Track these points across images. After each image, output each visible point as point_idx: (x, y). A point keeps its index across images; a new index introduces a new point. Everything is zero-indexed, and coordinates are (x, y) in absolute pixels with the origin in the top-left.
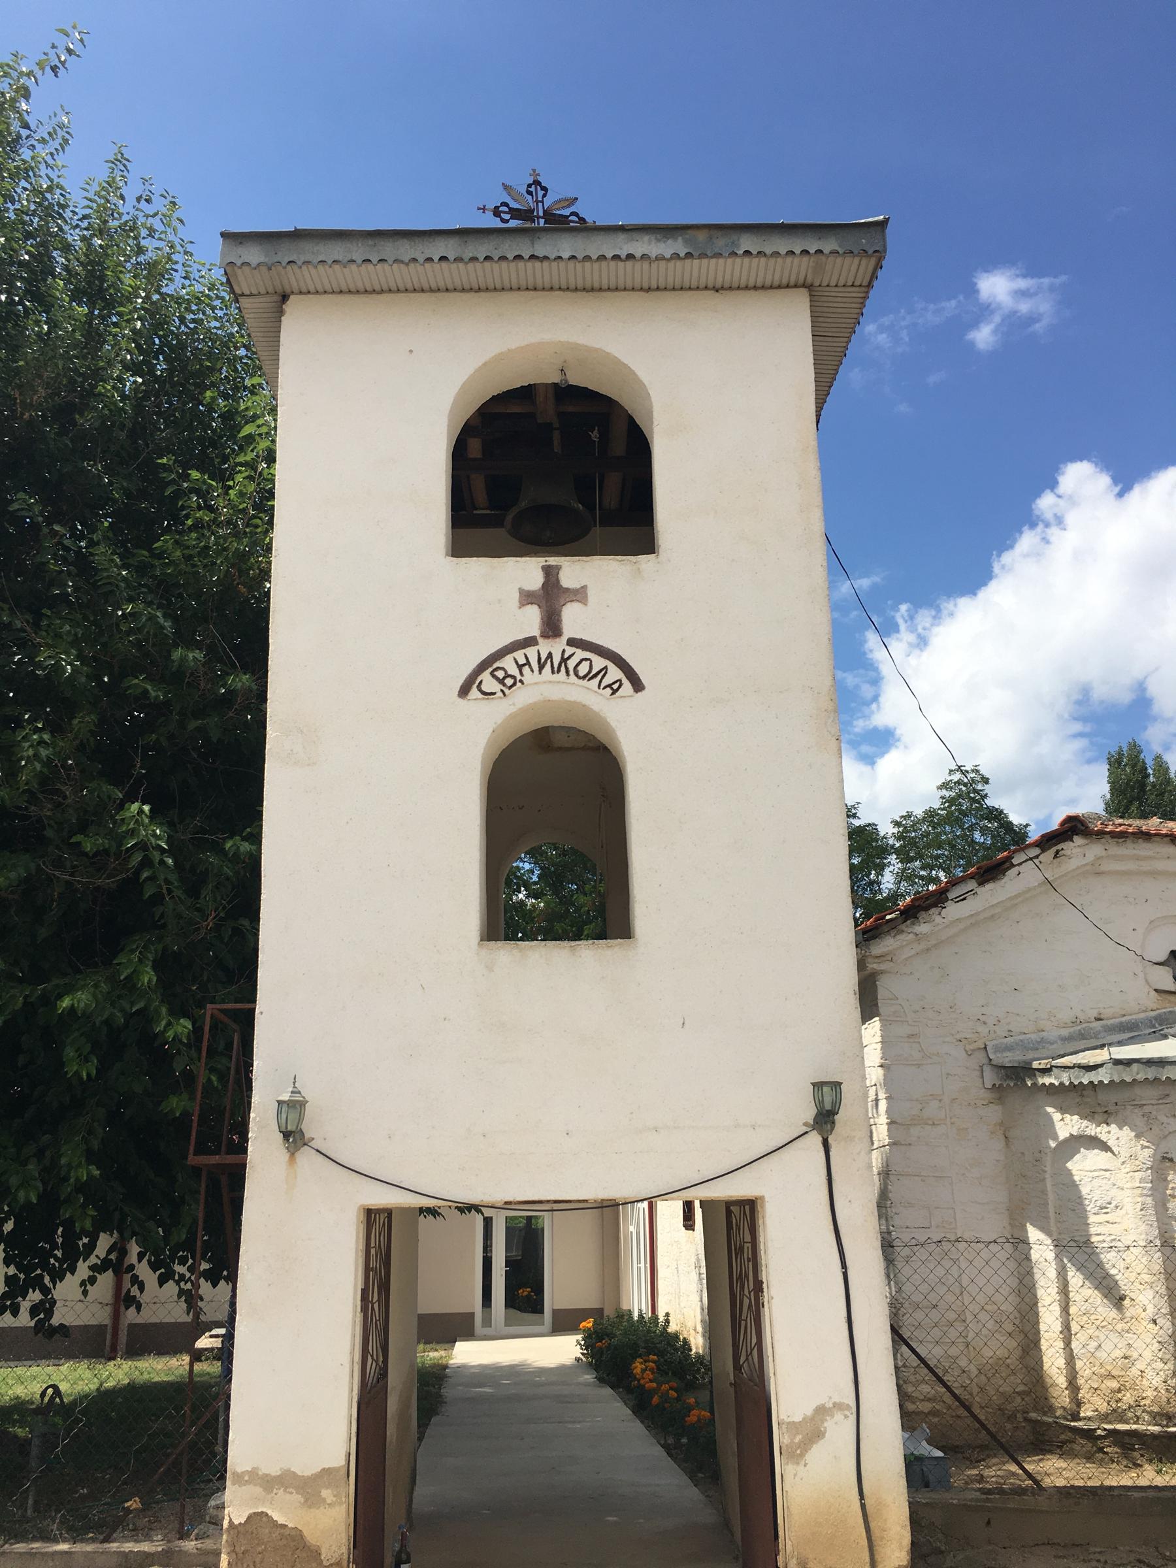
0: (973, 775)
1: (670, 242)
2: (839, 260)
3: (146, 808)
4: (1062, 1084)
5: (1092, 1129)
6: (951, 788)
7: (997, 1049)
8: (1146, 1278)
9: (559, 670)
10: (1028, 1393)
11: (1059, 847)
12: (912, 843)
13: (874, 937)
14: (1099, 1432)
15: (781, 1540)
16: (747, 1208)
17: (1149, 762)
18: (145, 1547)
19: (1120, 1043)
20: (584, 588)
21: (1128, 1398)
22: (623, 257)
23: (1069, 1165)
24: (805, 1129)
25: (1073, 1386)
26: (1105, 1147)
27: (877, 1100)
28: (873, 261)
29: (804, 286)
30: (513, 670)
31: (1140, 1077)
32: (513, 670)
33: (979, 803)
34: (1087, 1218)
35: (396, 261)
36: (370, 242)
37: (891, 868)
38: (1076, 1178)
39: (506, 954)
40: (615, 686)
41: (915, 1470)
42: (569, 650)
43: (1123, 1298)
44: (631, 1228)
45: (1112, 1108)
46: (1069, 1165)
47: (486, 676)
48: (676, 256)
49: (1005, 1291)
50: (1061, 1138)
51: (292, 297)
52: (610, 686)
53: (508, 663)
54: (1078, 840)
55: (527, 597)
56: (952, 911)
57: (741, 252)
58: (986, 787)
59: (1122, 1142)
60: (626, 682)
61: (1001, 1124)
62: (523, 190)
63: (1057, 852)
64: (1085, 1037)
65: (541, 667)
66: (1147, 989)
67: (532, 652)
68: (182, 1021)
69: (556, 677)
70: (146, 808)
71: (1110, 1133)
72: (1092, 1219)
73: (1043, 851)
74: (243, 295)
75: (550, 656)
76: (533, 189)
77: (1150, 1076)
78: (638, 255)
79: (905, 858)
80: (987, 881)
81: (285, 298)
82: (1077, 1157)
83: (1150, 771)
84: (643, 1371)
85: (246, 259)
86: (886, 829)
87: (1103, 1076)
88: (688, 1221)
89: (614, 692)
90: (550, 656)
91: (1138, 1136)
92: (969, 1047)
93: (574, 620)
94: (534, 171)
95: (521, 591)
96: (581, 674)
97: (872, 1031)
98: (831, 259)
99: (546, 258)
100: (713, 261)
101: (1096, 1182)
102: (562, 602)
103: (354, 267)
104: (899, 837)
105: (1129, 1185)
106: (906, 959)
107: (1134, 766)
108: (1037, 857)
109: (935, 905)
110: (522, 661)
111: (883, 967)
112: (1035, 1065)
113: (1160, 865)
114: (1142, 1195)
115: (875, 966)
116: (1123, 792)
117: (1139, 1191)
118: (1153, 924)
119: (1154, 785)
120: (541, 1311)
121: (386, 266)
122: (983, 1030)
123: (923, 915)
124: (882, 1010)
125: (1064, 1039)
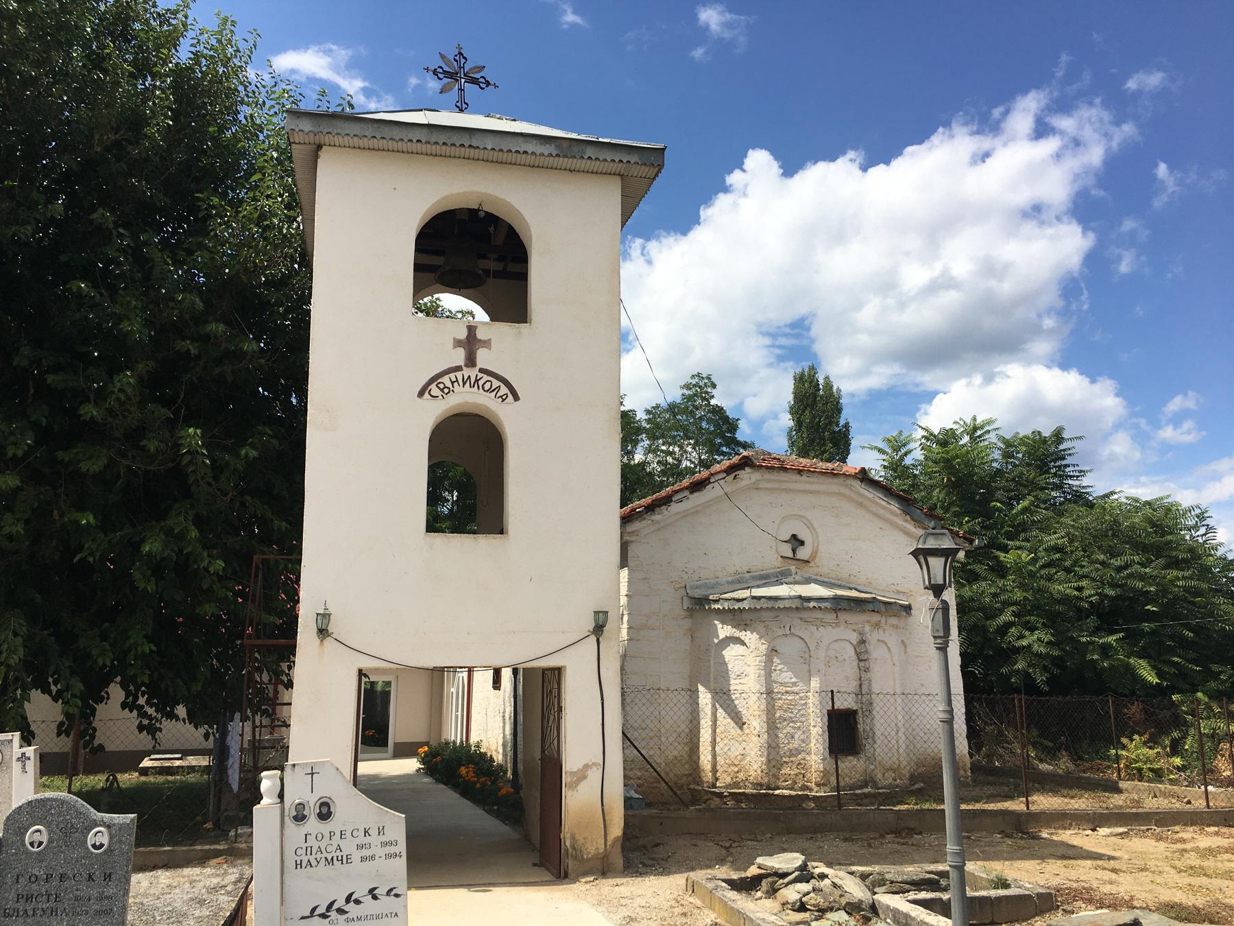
0: (706, 381)
1: (547, 146)
2: (639, 167)
3: (198, 431)
4: (724, 608)
5: (737, 634)
6: (690, 389)
7: (692, 588)
8: (757, 713)
9: (474, 386)
10: (690, 775)
11: (737, 473)
12: (658, 426)
13: (629, 521)
14: (725, 794)
15: (563, 826)
16: (556, 672)
17: (821, 381)
18: (218, 847)
19: (758, 586)
20: (490, 340)
21: (741, 775)
22: (521, 152)
23: (724, 653)
24: (588, 634)
25: (714, 770)
26: (743, 643)
27: (623, 615)
28: (657, 169)
29: (619, 175)
30: (449, 384)
31: (764, 606)
32: (449, 384)
33: (707, 400)
34: (729, 681)
35: (391, 139)
36: (376, 126)
37: (642, 444)
38: (727, 660)
39: (438, 539)
40: (504, 397)
41: (628, 802)
42: (480, 375)
43: (744, 724)
44: (452, 690)
45: (749, 622)
46: (724, 653)
47: (433, 386)
48: (551, 155)
49: (683, 718)
50: (720, 638)
51: (324, 147)
52: (501, 397)
53: (446, 380)
54: (748, 470)
55: (458, 343)
56: (675, 508)
57: (586, 157)
58: (714, 390)
59: (752, 641)
60: (509, 394)
61: (690, 629)
62: (452, 59)
63: (736, 476)
64: (740, 582)
65: (464, 384)
66: (776, 556)
67: (459, 375)
68: (218, 561)
69: (472, 389)
70: (198, 431)
71: (747, 636)
72: (732, 682)
73: (728, 475)
74: (294, 143)
75: (469, 377)
76: (457, 58)
77: (770, 606)
78: (530, 152)
79: (653, 438)
80: (695, 491)
81: (319, 147)
82: (728, 648)
83: (821, 387)
84: (467, 772)
85: (301, 127)
86: (641, 415)
87: (746, 605)
88: (497, 683)
89: (503, 400)
90: (469, 377)
91: (760, 638)
92: (677, 586)
93: (484, 358)
94: (459, 45)
95: (454, 339)
96: (486, 389)
97: (625, 573)
98: (634, 166)
99: (478, 147)
100: (571, 160)
101: (737, 662)
102: (477, 347)
103: (366, 139)
104: (648, 421)
105: (754, 664)
106: (646, 535)
107: (811, 383)
108: (724, 478)
109: (664, 504)
110: (454, 379)
111: (632, 539)
112: (711, 597)
113: (791, 486)
114: (759, 669)
115: (628, 538)
116: (802, 401)
117: (758, 667)
118: (783, 519)
119: (822, 397)
120: (385, 744)
121: (385, 141)
122: (685, 577)
123: (657, 509)
124: (629, 564)
125: (729, 583)
